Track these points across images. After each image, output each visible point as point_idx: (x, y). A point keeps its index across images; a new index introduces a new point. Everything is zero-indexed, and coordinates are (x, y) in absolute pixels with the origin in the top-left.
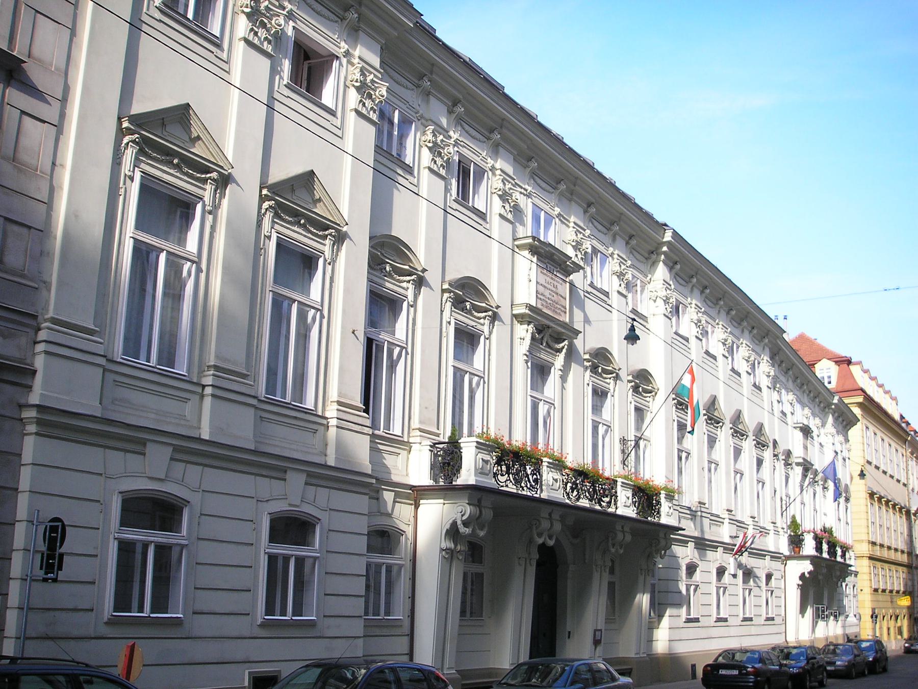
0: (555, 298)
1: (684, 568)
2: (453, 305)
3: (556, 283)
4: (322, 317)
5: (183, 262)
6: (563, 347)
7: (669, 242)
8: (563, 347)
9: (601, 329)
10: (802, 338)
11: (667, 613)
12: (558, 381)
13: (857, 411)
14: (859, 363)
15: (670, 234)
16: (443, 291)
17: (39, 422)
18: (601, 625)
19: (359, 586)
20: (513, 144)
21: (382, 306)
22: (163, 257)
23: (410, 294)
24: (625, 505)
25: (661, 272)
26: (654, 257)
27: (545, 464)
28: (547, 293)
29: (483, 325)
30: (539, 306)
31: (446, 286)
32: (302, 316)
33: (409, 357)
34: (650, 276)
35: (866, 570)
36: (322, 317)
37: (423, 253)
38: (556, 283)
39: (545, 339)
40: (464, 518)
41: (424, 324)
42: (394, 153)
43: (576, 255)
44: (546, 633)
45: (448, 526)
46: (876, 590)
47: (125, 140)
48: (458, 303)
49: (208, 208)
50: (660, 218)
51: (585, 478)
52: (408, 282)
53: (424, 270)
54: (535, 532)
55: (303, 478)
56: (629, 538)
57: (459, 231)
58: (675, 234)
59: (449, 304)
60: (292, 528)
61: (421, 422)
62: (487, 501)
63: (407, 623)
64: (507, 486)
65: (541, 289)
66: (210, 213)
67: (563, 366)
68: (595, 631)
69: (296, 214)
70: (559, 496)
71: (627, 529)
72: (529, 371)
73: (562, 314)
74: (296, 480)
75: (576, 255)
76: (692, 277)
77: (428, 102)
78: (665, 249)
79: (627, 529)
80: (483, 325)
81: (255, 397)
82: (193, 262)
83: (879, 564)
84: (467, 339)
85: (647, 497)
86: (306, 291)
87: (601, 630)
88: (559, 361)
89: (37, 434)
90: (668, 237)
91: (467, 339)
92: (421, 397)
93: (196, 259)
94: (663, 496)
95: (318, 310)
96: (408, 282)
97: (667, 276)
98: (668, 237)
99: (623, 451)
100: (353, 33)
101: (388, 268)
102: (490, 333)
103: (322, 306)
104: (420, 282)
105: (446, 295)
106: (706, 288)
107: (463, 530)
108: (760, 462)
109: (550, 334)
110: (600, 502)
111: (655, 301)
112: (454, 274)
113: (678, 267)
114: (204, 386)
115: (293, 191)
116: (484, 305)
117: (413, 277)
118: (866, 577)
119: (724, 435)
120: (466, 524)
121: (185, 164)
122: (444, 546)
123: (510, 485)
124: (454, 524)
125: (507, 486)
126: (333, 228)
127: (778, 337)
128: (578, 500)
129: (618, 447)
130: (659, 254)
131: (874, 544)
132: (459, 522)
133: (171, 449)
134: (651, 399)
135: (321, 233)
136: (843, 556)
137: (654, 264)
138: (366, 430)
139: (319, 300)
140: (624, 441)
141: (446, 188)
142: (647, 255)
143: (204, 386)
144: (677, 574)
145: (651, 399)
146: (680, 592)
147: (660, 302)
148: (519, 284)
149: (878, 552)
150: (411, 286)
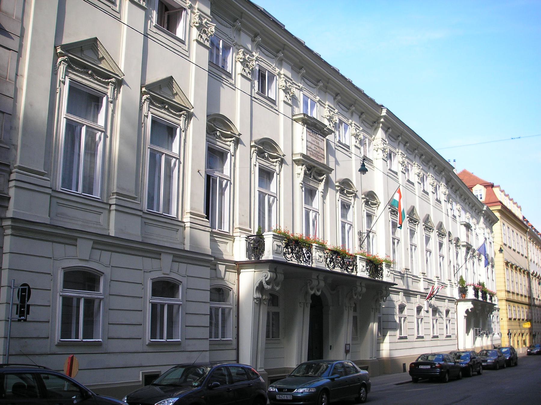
0: (318, 150)
1: (397, 307)
2: (257, 154)
3: (318, 141)
4: (180, 163)
5: (171, 158)
6: (323, 179)
7: (384, 116)
8: (323, 179)
9: (345, 167)
10: (464, 172)
11: (388, 334)
12: (321, 198)
13: (497, 214)
14: (498, 186)
15: (385, 111)
16: (251, 147)
17: (13, 228)
18: (349, 341)
19: (206, 321)
20: (251, 31)
21: (215, 156)
22: (84, 129)
23: (232, 149)
24: (362, 271)
25: (380, 134)
26: (376, 125)
27: (314, 247)
28: (313, 147)
29: (275, 166)
30: (309, 155)
31: (253, 144)
32: (168, 163)
33: (232, 186)
34: (374, 136)
35: (504, 307)
36: (180, 163)
37: (239, 124)
38: (318, 141)
39: (313, 174)
40: (267, 279)
41: (240, 166)
42: (220, 66)
43: (330, 125)
44: (317, 346)
45: (257, 285)
46: (510, 319)
47: (60, 60)
48: (260, 153)
49: (110, 100)
50: (379, 102)
51: (338, 255)
52: (231, 141)
53: (240, 134)
54: (309, 287)
55: (171, 257)
56: (364, 290)
57: (260, 110)
58: (388, 111)
59: (255, 154)
60: (165, 287)
61: (240, 224)
62: (280, 269)
63: (235, 342)
64: (292, 260)
65: (309, 144)
66: (111, 102)
67: (323, 190)
68: (346, 345)
69: (163, 102)
70: (323, 266)
71: (363, 285)
72: (303, 193)
73: (322, 159)
74: (167, 260)
75: (330, 125)
76: (399, 136)
77: (239, 35)
78: (382, 120)
79: (363, 285)
80: (275, 166)
81: (141, 211)
82: (102, 131)
83: (512, 304)
84: (266, 175)
85: (374, 266)
86: (170, 148)
87: (349, 344)
88: (321, 187)
89: (12, 235)
90: (384, 113)
91: (266, 175)
92: (240, 209)
93: (104, 130)
94: (384, 265)
95: (177, 159)
96: (231, 141)
97: (384, 136)
98: (384, 113)
99: (360, 240)
100: (280, 63)
101: (218, 134)
102: (280, 171)
103: (180, 156)
104: (237, 142)
105: (253, 149)
106: (407, 143)
107: (266, 286)
108: (441, 245)
109: (315, 171)
110: (347, 269)
111: (377, 151)
112: (257, 137)
113: (390, 130)
114: (110, 205)
115: (160, 88)
116: (229, 133)
117: (233, 139)
118: (504, 311)
119: (419, 229)
120: (268, 283)
121: (153, 99)
122: (255, 296)
123: (294, 260)
124: (261, 283)
125: (292, 260)
126: (235, 137)
127: (450, 171)
128: (334, 268)
129: (357, 237)
130: (379, 123)
131: (509, 292)
132: (264, 282)
133: (92, 242)
134: (376, 209)
135: (178, 113)
136: (491, 299)
137: (376, 129)
138: (208, 229)
139: (178, 153)
140: (360, 233)
141: (251, 86)
142: (371, 124)
143: (110, 205)
144: (394, 311)
145: (376, 209)
146: (396, 322)
147: (380, 152)
148: (297, 142)
149: (511, 297)
150: (232, 144)
